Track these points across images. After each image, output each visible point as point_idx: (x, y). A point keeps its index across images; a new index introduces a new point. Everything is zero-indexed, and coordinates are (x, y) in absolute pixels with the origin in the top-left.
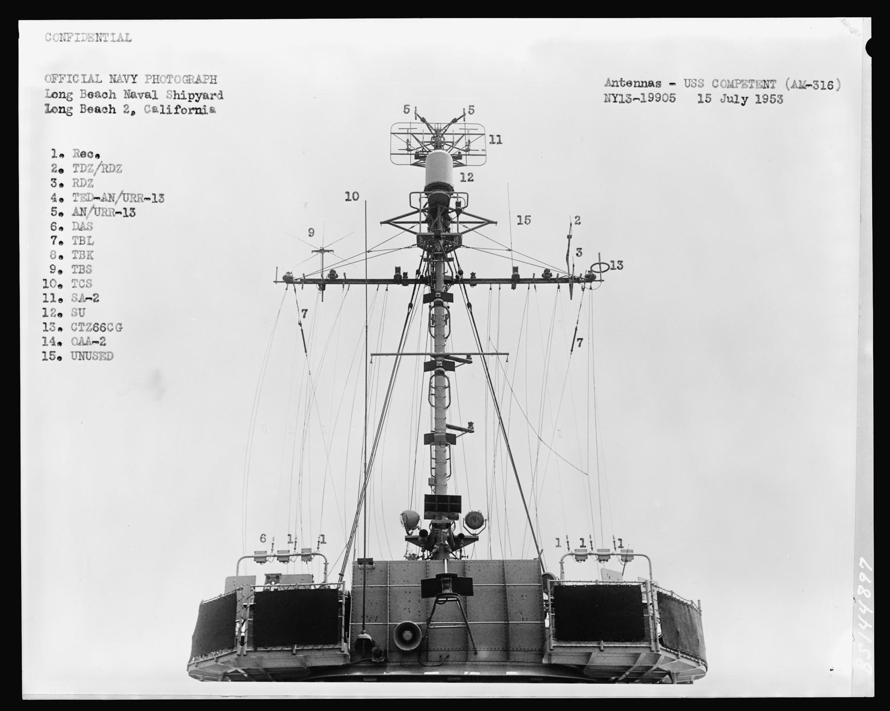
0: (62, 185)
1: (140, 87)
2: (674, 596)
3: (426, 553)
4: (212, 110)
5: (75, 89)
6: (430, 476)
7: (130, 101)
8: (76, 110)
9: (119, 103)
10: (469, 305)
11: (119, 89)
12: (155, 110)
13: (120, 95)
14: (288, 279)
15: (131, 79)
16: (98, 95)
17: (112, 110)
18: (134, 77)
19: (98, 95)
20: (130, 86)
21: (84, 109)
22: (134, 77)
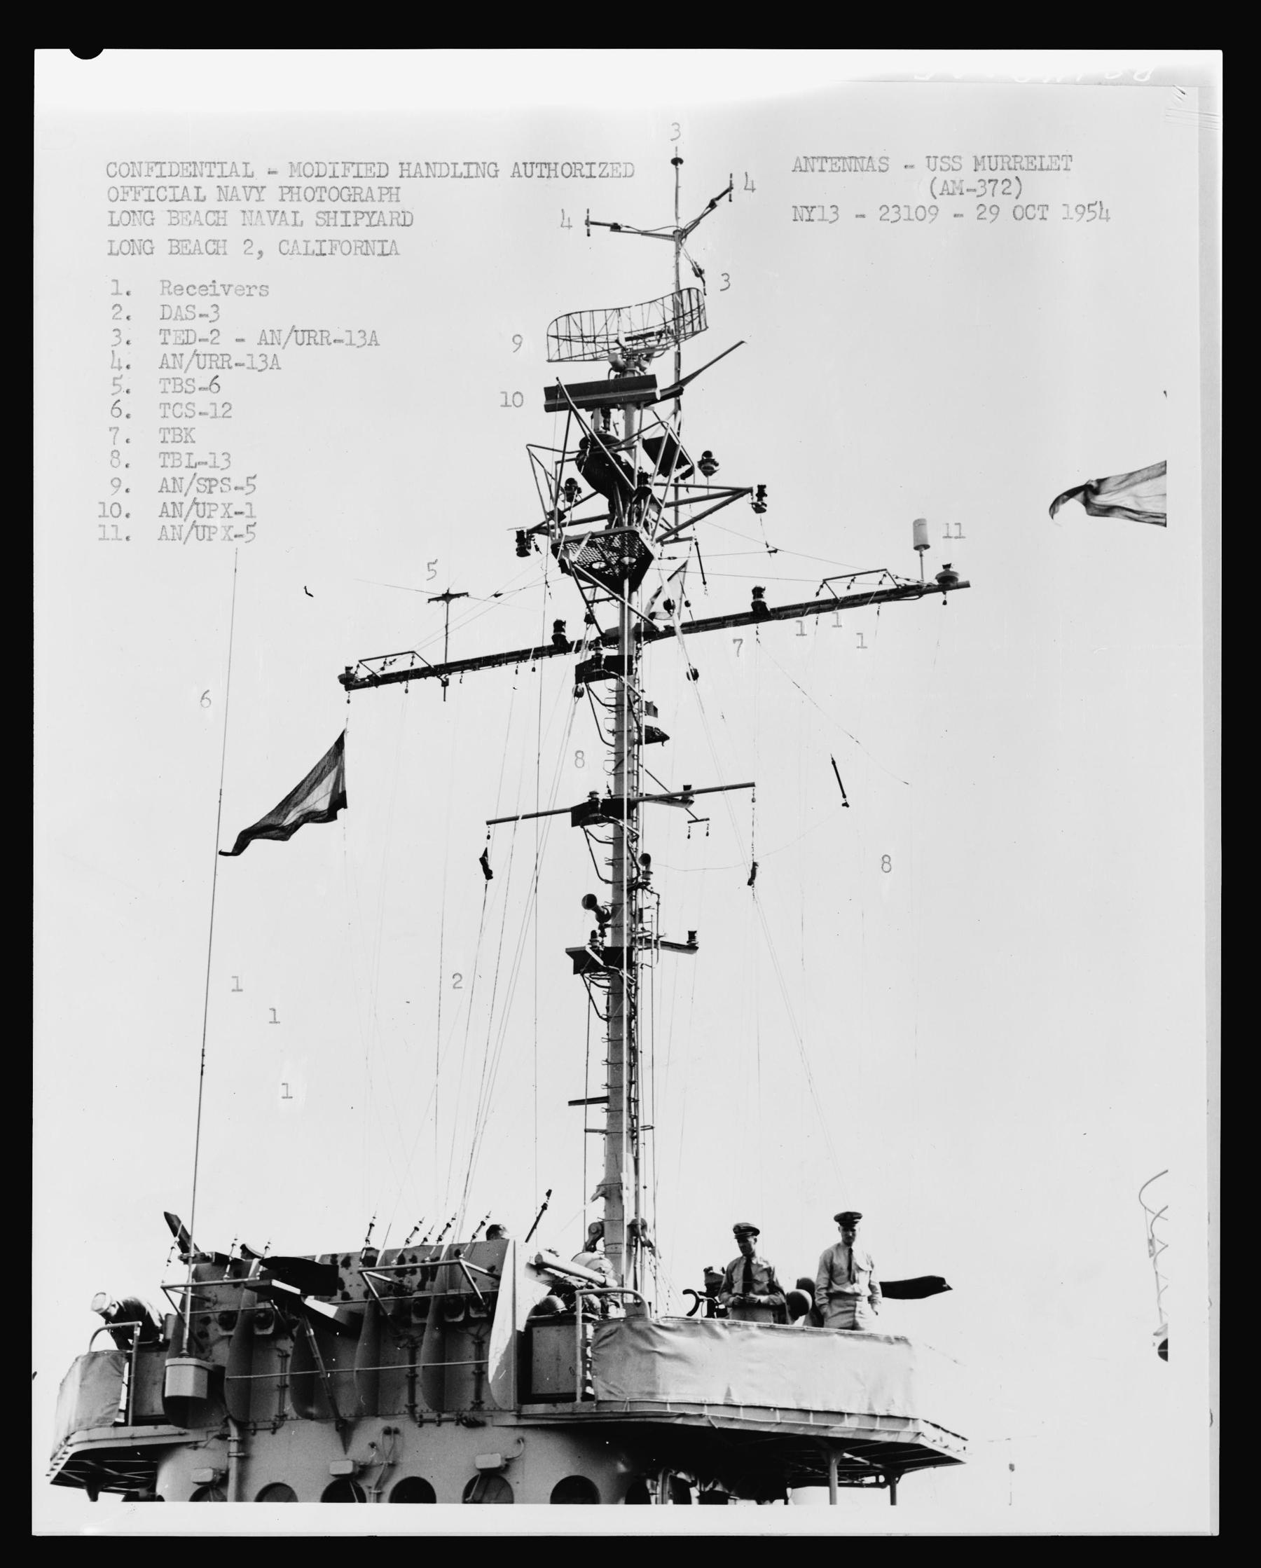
8: (162, 247)
13: (234, 217)
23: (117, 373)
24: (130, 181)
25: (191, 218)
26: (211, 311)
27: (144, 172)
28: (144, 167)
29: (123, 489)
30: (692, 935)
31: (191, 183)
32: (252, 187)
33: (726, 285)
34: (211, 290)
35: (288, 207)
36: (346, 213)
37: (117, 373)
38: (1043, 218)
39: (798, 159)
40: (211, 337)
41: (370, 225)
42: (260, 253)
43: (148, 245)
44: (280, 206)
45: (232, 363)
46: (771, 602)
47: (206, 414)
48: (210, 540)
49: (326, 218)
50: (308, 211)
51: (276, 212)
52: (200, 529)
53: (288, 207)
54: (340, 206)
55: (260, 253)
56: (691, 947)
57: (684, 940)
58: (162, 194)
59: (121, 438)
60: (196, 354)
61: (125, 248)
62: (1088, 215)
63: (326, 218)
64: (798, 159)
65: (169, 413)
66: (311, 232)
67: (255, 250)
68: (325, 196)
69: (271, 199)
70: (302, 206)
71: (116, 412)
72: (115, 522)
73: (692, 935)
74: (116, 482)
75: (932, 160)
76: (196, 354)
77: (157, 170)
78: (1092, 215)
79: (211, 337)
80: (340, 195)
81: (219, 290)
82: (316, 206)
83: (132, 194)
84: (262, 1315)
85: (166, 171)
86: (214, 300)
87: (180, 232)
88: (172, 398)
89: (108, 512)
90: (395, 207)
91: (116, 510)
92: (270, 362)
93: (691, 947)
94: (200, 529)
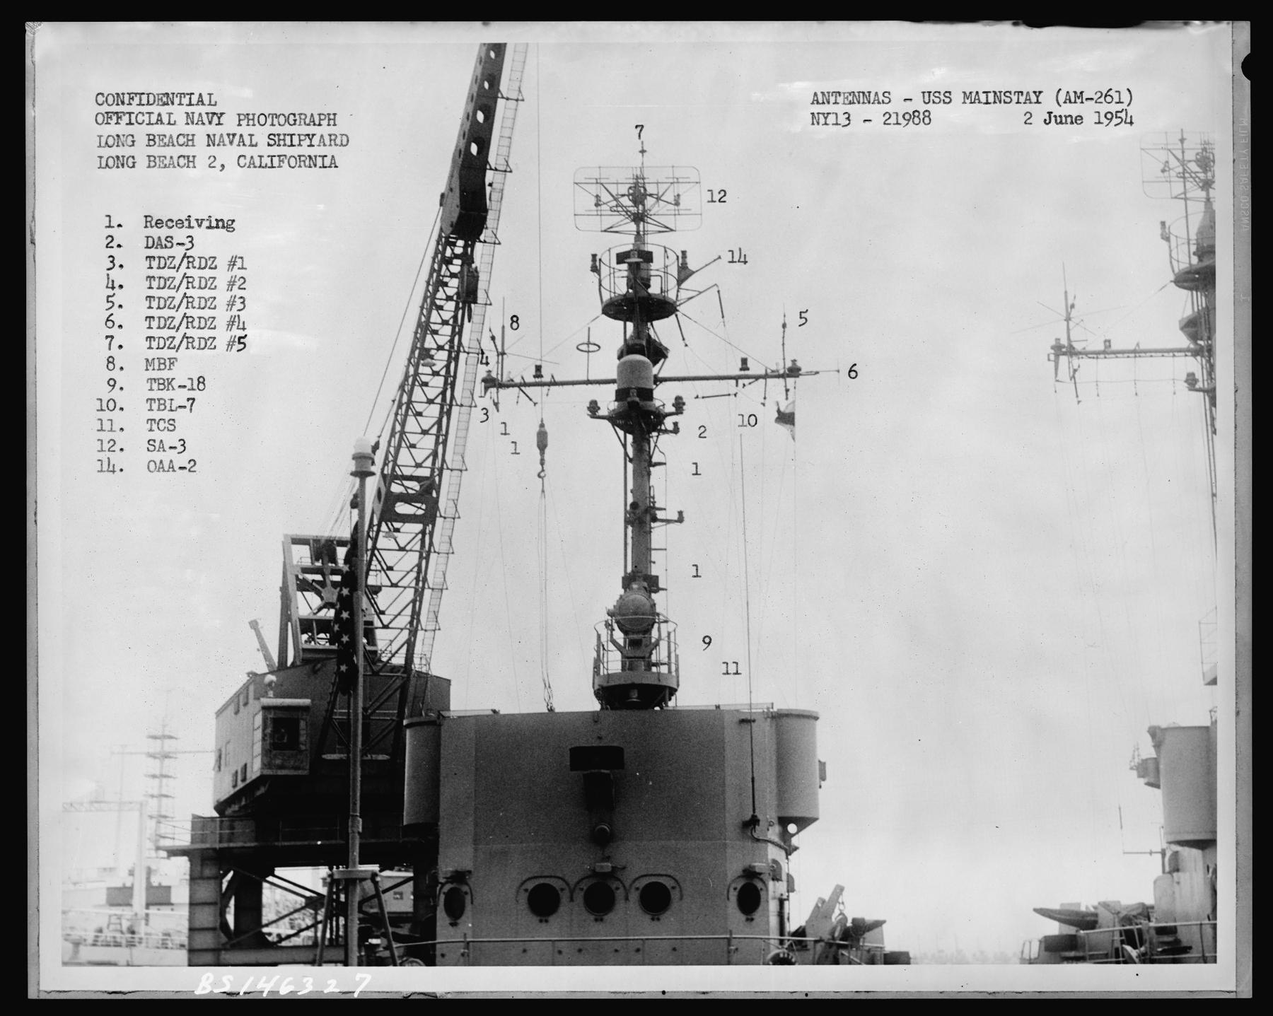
7: (213, 150)
8: (142, 162)
12: (252, 164)
13: (201, 140)
15: (215, 120)
21: (152, 161)
23: (110, 292)
24: (115, 108)
25: (166, 140)
26: (187, 241)
27: (126, 101)
28: (127, 97)
29: (117, 387)
30: (680, 513)
31: (164, 110)
34: (186, 224)
35: (245, 130)
36: (291, 135)
37: (110, 292)
39: (815, 94)
40: (188, 466)
42: (223, 166)
43: (131, 160)
44: (238, 131)
46: (734, 382)
49: (274, 140)
50: (261, 134)
51: (234, 135)
53: (245, 130)
54: (288, 129)
55: (223, 166)
56: (681, 519)
57: (676, 517)
58: (140, 118)
59: (115, 344)
61: (111, 162)
62: (1115, 121)
63: (274, 140)
64: (815, 94)
65: (155, 427)
67: (217, 164)
68: (276, 121)
69: (230, 124)
70: (256, 130)
71: (110, 324)
72: (112, 436)
73: (680, 513)
74: (112, 383)
77: (137, 100)
79: (188, 466)
80: (287, 120)
81: (194, 223)
82: (268, 129)
83: (115, 118)
84: (262, 790)
85: (146, 117)
86: (190, 232)
87: (156, 151)
88: (157, 415)
90: (332, 130)
91: (111, 405)
93: (681, 519)
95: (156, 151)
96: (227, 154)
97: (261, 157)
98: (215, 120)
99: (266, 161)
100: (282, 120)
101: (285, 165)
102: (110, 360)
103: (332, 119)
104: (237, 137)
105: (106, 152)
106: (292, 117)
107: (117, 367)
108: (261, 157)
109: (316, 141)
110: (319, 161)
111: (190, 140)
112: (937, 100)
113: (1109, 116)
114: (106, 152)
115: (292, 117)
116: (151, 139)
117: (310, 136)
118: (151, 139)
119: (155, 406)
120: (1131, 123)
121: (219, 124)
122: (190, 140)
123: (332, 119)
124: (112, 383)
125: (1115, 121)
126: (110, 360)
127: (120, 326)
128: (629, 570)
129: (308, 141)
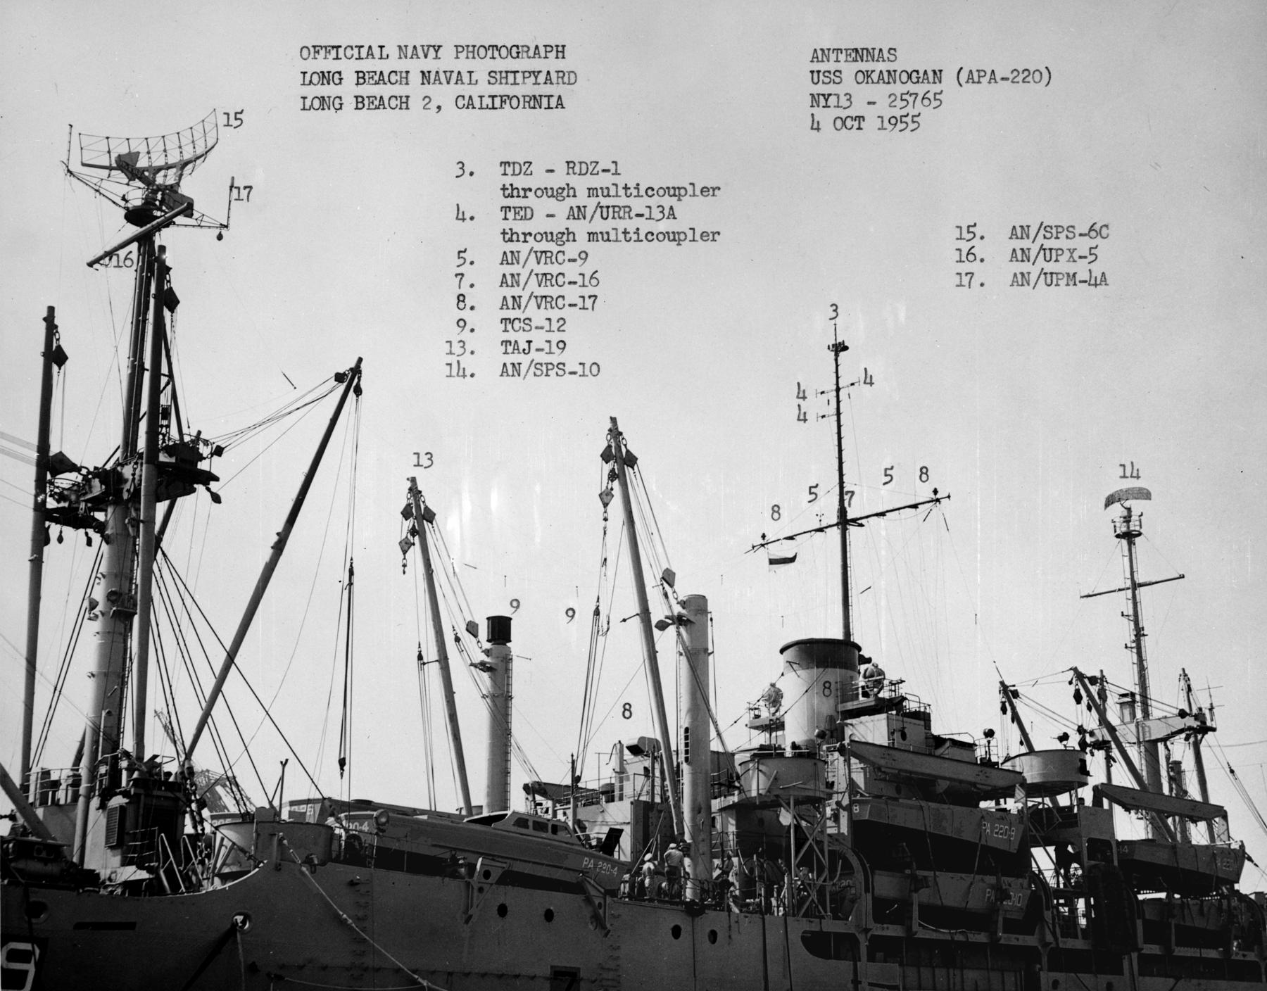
0: (472, 308)
1: (447, 61)
2: (99, 594)
3: (229, 836)
4: (560, 104)
5: (348, 68)
6: (100, 466)
7: (430, 89)
8: (349, 102)
9: (415, 89)
10: (1232, 771)
11: (415, 67)
12: (470, 105)
13: (415, 78)
14: (156, 208)
15: (432, 53)
16: (381, 79)
17: (404, 102)
18: (437, 48)
19: (381, 79)
20: (430, 64)
21: (360, 101)
22: (437, 48)
32: (429, 46)
33: (834, 314)
38: (859, 128)
41: (536, 83)
42: (439, 107)
43: (337, 101)
45: (632, 214)
47: (575, 283)
48: (1057, 261)
50: (482, 67)
52: (1048, 252)
54: (511, 64)
60: (599, 206)
61: (316, 104)
62: (900, 126)
66: (484, 88)
67: (433, 106)
75: (815, 75)
76: (599, 206)
78: (904, 126)
87: (366, 90)
89: (587, 372)
92: (666, 212)
94: (1048, 252)
95: (366, 90)
96: (444, 94)
97: (481, 97)
98: (432, 53)
99: (487, 101)
100: (504, 52)
101: (507, 106)
102: (461, 298)
103: (560, 51)
104: (454, 76)
105: (312, 91)
106: (514, 50)
107: (468, 307)
108: (481, 97)
109: (542, 78)
110: (545, 101)
111: (405, 77)
112: (827, 80)
113: (893, 121)
114: (312, 91)
115: (514, 50)
116: (361, 77)
117: (536, 74)
118: (361, 77)
119: (510, 349)
120: (871, 384)
121: (437, 57)
122: (405, 77)
123: (560, 51)
124: (462, 323)
125: (900, 126)
126: (461, 298)
127: (982, 260)
128: (108, 467)
129: (532, 79)
